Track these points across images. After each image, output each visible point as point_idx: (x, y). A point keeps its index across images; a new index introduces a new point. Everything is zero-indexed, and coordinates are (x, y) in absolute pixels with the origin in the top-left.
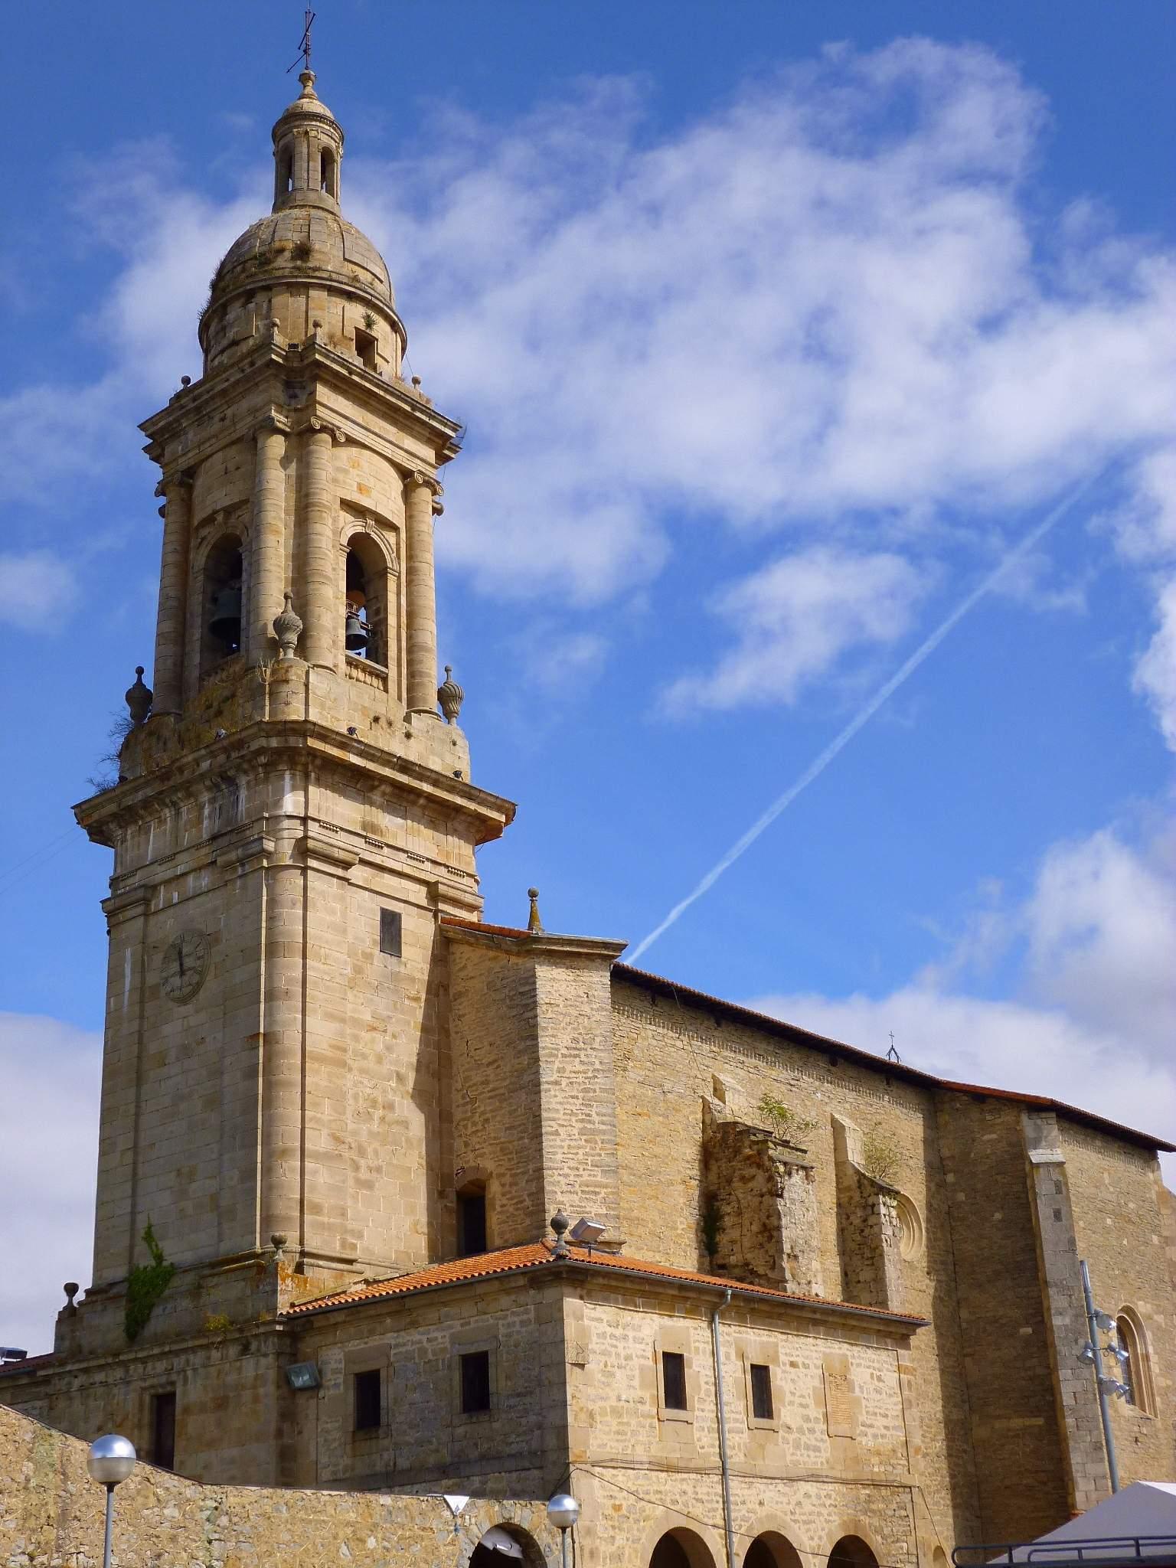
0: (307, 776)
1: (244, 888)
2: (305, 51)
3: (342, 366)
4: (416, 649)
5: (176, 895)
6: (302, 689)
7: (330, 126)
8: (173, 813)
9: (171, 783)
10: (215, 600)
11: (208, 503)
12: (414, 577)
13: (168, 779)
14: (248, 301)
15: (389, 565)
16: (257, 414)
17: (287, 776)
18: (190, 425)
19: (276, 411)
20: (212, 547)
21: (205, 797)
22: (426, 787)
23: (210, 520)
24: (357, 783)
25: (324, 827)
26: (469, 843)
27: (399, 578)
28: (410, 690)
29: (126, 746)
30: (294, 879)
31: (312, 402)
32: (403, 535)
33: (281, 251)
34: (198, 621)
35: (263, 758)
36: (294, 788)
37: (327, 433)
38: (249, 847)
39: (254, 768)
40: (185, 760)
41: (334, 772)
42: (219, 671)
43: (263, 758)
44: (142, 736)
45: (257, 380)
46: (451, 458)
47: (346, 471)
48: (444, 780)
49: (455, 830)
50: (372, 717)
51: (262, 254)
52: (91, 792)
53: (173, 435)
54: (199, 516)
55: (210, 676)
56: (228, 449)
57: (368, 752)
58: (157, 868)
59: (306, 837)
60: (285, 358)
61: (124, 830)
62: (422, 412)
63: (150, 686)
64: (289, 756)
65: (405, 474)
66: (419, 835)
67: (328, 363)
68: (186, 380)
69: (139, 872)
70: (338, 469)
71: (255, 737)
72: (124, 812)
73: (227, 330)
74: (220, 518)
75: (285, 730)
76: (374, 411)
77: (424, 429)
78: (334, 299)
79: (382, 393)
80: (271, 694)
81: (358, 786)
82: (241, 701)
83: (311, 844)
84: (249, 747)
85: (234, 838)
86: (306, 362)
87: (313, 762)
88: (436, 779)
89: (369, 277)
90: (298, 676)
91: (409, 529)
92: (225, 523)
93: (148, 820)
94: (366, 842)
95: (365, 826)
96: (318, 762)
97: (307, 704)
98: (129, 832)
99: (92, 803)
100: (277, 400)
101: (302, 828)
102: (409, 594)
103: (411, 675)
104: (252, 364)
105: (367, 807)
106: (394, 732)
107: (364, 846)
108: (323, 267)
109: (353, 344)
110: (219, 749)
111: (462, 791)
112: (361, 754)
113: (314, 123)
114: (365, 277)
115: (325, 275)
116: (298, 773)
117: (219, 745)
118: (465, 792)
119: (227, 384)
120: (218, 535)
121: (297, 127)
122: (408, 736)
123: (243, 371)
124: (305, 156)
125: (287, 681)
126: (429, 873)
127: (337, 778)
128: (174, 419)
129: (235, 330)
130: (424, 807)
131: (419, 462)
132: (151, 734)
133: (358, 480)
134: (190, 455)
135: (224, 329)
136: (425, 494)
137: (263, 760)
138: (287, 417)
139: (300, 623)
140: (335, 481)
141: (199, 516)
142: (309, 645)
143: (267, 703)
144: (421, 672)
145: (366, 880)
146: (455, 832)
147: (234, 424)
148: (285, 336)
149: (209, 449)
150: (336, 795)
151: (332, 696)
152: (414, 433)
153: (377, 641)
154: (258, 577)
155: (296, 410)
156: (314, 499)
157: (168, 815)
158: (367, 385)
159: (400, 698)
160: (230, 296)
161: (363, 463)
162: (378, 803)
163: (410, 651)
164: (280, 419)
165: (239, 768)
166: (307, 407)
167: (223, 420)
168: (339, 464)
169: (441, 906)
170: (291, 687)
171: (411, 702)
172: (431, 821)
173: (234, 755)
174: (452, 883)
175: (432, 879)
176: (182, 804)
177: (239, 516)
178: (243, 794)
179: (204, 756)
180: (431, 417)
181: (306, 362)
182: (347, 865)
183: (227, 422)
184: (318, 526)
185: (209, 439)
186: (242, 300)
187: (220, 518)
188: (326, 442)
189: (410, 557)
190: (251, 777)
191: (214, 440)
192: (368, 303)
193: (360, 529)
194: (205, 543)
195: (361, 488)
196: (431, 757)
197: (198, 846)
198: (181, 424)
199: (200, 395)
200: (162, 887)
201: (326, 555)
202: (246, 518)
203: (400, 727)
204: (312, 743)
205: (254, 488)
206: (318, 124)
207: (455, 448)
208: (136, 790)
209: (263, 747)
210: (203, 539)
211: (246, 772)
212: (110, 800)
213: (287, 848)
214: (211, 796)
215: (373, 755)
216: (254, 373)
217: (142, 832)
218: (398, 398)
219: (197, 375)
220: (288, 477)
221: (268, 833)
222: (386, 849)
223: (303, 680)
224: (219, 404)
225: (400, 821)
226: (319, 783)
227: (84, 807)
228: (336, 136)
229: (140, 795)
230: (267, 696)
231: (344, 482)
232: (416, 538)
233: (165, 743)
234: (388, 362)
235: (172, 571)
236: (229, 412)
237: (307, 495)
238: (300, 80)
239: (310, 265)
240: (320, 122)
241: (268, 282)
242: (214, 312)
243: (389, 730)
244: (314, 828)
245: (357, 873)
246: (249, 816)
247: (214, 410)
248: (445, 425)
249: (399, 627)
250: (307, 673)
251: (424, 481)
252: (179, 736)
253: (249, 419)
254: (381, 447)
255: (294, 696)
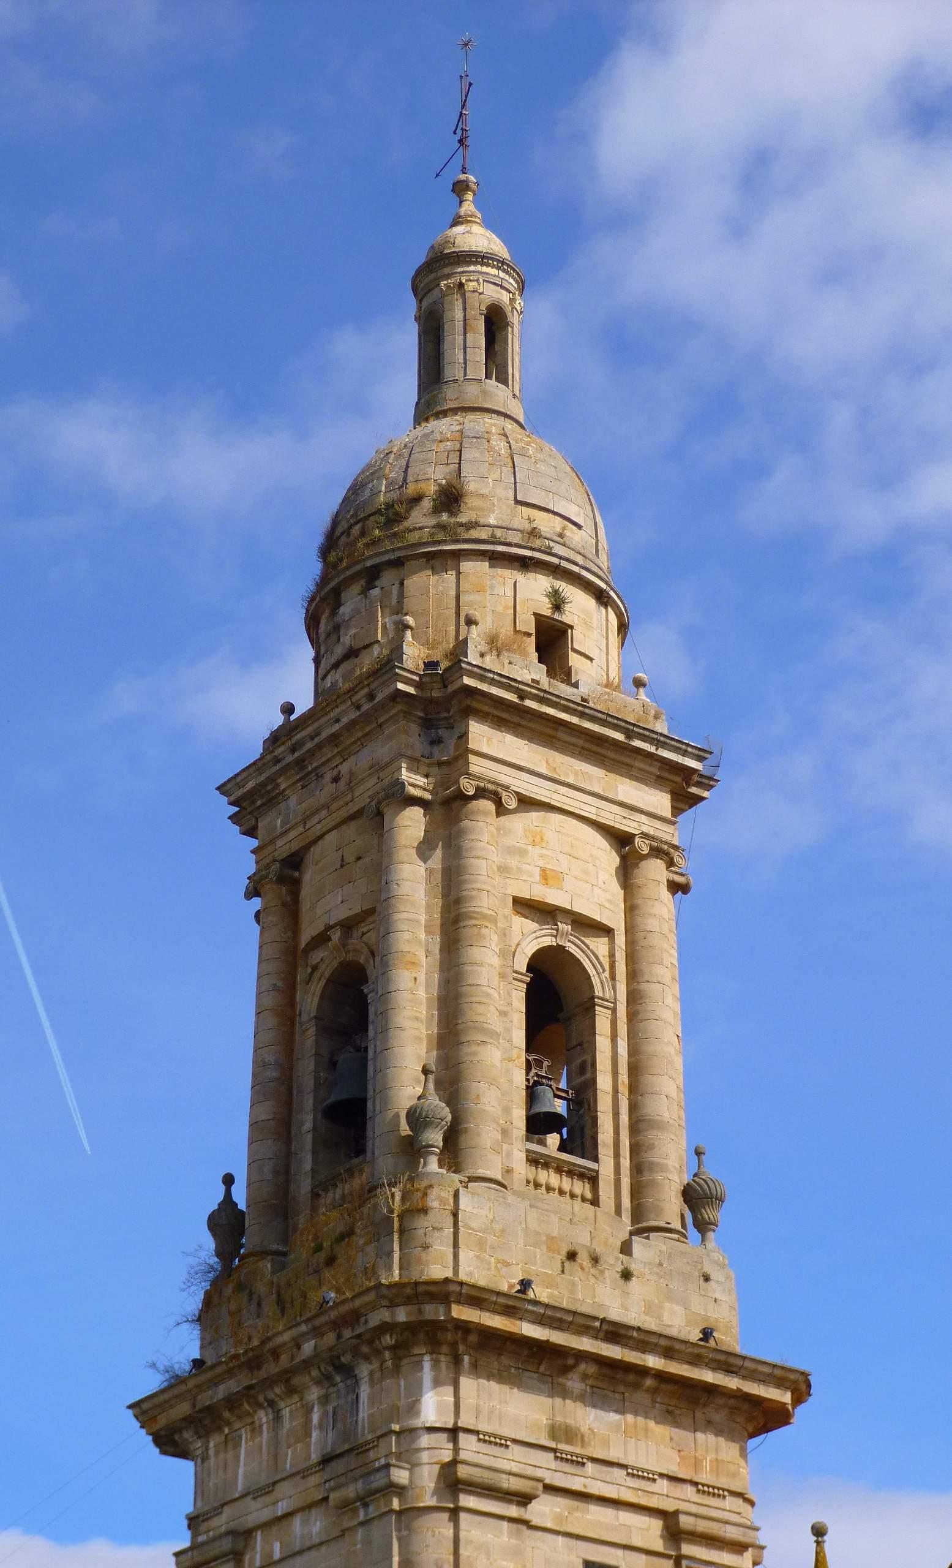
0: (457, 1361)
1: (367, 1542)
2: (461, 141)
3: (508, 688)
4: (642, 1126)
5: (277, 1547)
6: (450, 1220)
7: (499, 268)
8: (271, 1417)
9: (263, 1374)
10: (333, 1064)
11: (319, 913)
12: (639, 1007)
13: (259, 1367)
14: (370, 586)
15: (598, 992)
16: (382, 775)
17: (427, 1365)
18: (289, 787)
19: (409, 769)
20: (328, 980)
21: (314, 1394)
22: (653, 1361)
23: (322, 939)
24: (539, 1365)
25: (485, 1441)
26: (733, 1441)
27: (614, 1011)
28: (637, 1192)
29: (208, 1302)
30: (439, 1528)
31: (463, 752)
32: (620, 940)
33: (417, 499)
34: (309, 1102)
35: (388, 1337)
36: (437, 1383)
37: (488, 799)
38: (372, 1478)
39: (378, 1352)
40: (279, 1340)
41: (499, 1351)
42: (330, 1188)
43: (388, 1337)
44: (229, 1290)
45: (380, 721)
46: (703, 799)
47: (522, 852)
48: (682, 1347)
49: (709, 1422)
50: (564, 1252)
51: (389, 506)
52: (152, 1383)
53: (269, 801)
54: (307, 934)
55: (326, 1190)
56: (344, 827)
57: (551, 1317)
58: (250, 1504)
59: (455, 1462)
60: (418, 685)
61: (204, 1440)
62: (644, 738)
63: (242, 1206)
64: (427, 1333)
65: (621, 840)
66: (647, 1437)
67: (484, 687)
68: (288, 709)
69: (226, 1509)
70: (511, 851)
71: (373, 1307)
72: (201, 1415)
73: (342, 632)
74: (336, 935)
75: (417, 1295)
76: (564, 748)
77: (650, 765)
78: (500, 571)
79: (575, 720)
80: (402, 1231)
81: (542, 1369)
82: (361, 1242)
83: (462, 1471)
84: (366, 1322)
85: (352, 1461)
86: (451, 689)
87: (464, 1339)
88: (669, 1348)
89: (558, 524)
90: (443, 1201)
91: (630, 929)
92: (344, 945)
93: (237, 1425)
94: (556, 1458)
95: (554, 1432)
96: (473, 1338)
97: (456, 1245)
98: (212, 1444)
99: (156, 1400)
100: (409, 753)
101: (451, 1446)
102: (632, 1035)
103: (638, 1169)
104: (371, 697)
105: (558, 1401)
106: (602, 1272)
107: (553, 1464)
108: (482, 521)
109: (531, 643)
110: (326, 1323)
111: (713, 1360)
112: (540, 1320)
113: (472, 268)
114: (547, 525)
115: (484, 534)
116: (442, 1358)
117: (324, 1319)
118: (719, 1362)
119: (337, 727)
120: (335, 964)
121: (448, 276)
122: (626, 1275)
123: (358, 707)
124: (459, 325)
125: (425, 1211)
126: (663, 1495)
127: (505, 1360)
128: (268, 778)
129: (353, 631)
130: (654, 1391)
131: (643, 818)
132: (240, 1287)
133: (541, 863)
134: (292, 834)
135: (337, 628)
136: (655, 872)
137: (388, 1340)
138: (427, 776)
139: (446, 1113)
140: (503, 869)
141: (307, 934)
142: (463, 1145)
143: (396, 1246)
144: (652, 1163)
145: (559, 1518)
146: (709, 1426)
147: (352, 789)
148: (426, 643)
149: (319, 826)
150: (506, 1388)
151: (498, 1227)
152: (634, 772)
153: (582, 1116)
154: (386, 1040)
155: (440, 764)
156: (467, 908)
157: (264, 1420)
158: (551, 711)
159: (618, 1211)
160: (342, 577)
161: (550, 836)
162: (575, 1391)
163: (635, 1128)
164: (415, 782)
165: (356, 1352)
166: (456, 759)
167: (336, 780)
168: (509, 841)
169: (687, 1549)
170: (432, 1218)
171: (637, 1214)
172: (668, 1412)
173: (347, 1333)
174: (703, 1511)
175: (669, 1506)
176: (282, 1404)
177: (364, 934)
178: (365, 1391)
179: (304, 1334)
180: (658, 744)
181: (451, 689)
182: (524, 1499)
183: (342, 782)
184: (475, 950)
185: (317, 811)
186: (363, 582)
187: (336, 935)
188: (485, 813)
189: (633, 975)
190: (376, 1365)
191: (324, 813)
192: (556, 571)
193: (548, 942)
194: (317, 975)
195: (546, 876)
196: (667, 1305)
197: (303, 1473)
198: (278, 785)
199: (300, 744)
200: (259, 1533)
201: (488, 995)
202: (371, 938)
203: (613, 1261)
204: (462, 1312)
205: (380, 891)
206: (479, 268)
207: (707, 782)
208: (215, 1382)
209: (386, 1323)
210: (315, 968)
211: (366, 1358)
212: (180, 1397)
213: (427, 1478)
214: (323, 1392)
215: (561, 1320)
216: (375, 709)
217: (230, 1446)
218: (603, 723)
219: (304, 703)
220: (430, 872)
221: (399, 1456)
222: (590, 1466)
223: (451, 1206)
224: (329, 755)
225: (614, 1417)
226: (476, 1370)
227: (145, 1406)
228: (511, 282)
229: (222, 1391)
230: (396, 1236)
231: (519, 870)
232: (642, 943)
233: (259, 1304)
234: (591, 659)
235: (271, 1021)
236: (344, 768)
237: (458, 901)
238: (453, 190)
239: (462, 519)
240: (482, 264)
241: (398, 554)
242: (323, 599)
243: (593, 1271)
244: (469, 1445)
245: (543, 1510)
246: (372, 1430)
247: (323, 764)
248: (685, 753)
249: (616, 1091)
250: (456, 1195)
251: (652, 849)
252: (279, 1294)
253: (374, 780)
254: (577, 804)
255: (437, 1234)
